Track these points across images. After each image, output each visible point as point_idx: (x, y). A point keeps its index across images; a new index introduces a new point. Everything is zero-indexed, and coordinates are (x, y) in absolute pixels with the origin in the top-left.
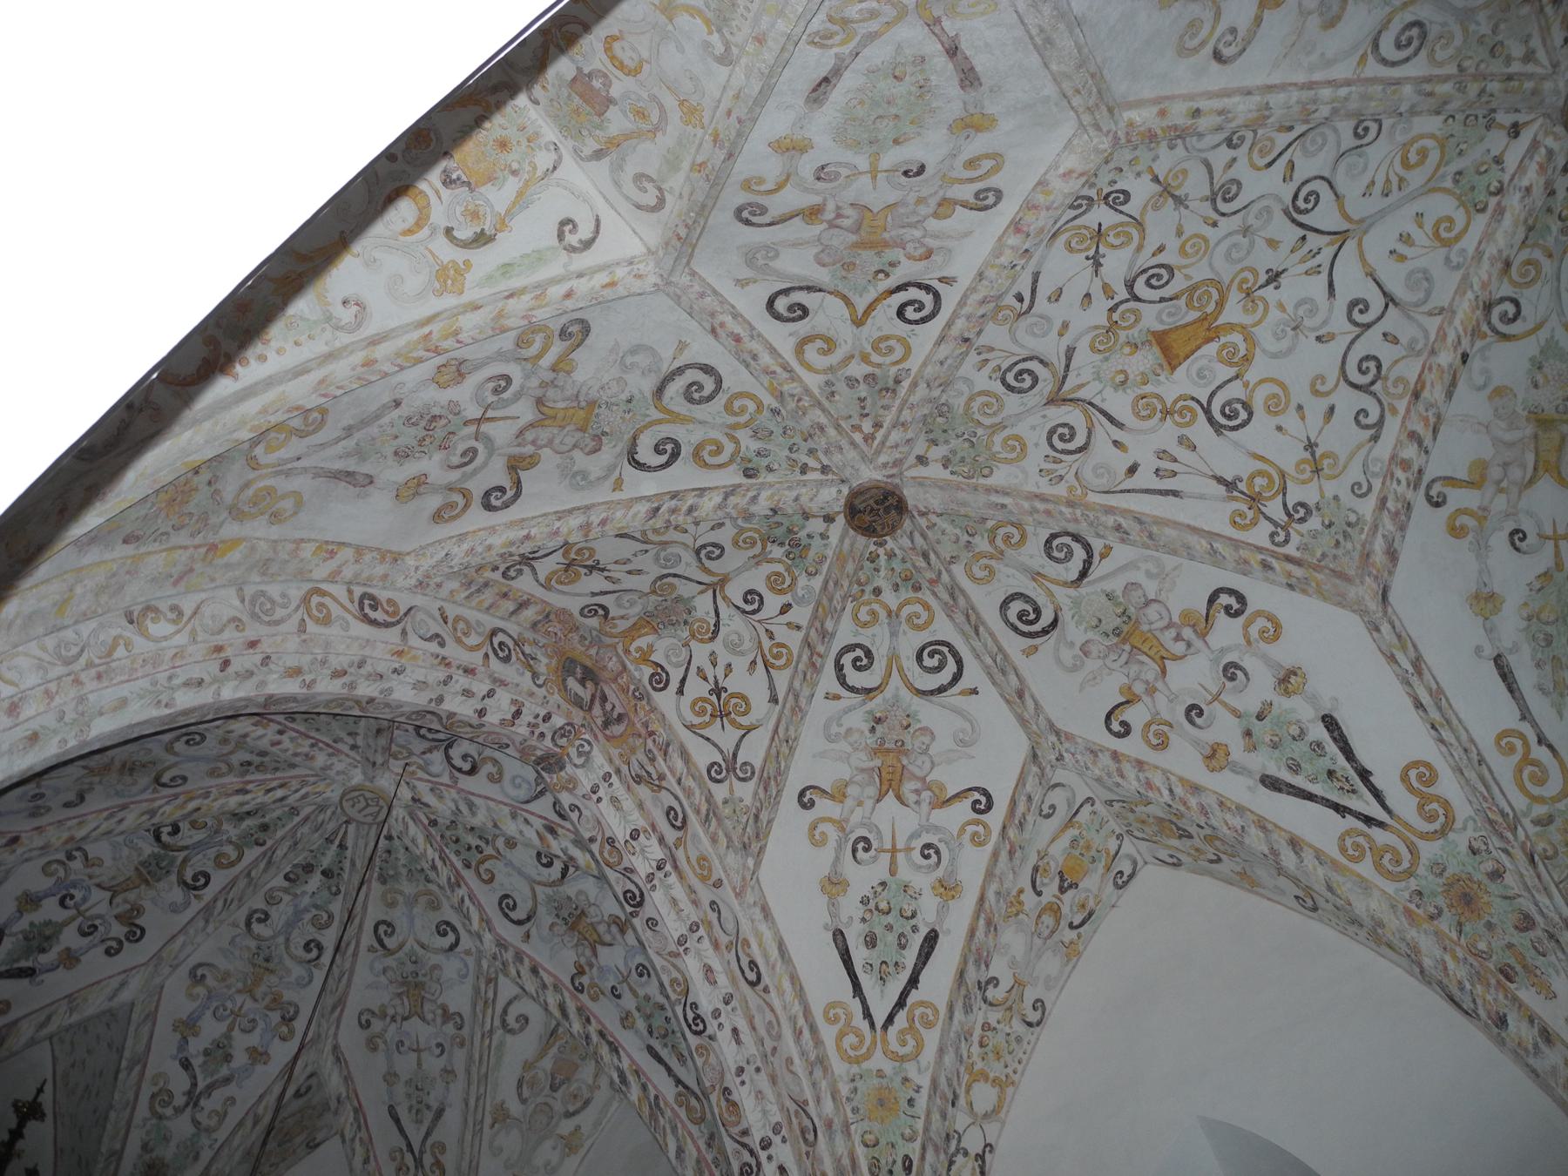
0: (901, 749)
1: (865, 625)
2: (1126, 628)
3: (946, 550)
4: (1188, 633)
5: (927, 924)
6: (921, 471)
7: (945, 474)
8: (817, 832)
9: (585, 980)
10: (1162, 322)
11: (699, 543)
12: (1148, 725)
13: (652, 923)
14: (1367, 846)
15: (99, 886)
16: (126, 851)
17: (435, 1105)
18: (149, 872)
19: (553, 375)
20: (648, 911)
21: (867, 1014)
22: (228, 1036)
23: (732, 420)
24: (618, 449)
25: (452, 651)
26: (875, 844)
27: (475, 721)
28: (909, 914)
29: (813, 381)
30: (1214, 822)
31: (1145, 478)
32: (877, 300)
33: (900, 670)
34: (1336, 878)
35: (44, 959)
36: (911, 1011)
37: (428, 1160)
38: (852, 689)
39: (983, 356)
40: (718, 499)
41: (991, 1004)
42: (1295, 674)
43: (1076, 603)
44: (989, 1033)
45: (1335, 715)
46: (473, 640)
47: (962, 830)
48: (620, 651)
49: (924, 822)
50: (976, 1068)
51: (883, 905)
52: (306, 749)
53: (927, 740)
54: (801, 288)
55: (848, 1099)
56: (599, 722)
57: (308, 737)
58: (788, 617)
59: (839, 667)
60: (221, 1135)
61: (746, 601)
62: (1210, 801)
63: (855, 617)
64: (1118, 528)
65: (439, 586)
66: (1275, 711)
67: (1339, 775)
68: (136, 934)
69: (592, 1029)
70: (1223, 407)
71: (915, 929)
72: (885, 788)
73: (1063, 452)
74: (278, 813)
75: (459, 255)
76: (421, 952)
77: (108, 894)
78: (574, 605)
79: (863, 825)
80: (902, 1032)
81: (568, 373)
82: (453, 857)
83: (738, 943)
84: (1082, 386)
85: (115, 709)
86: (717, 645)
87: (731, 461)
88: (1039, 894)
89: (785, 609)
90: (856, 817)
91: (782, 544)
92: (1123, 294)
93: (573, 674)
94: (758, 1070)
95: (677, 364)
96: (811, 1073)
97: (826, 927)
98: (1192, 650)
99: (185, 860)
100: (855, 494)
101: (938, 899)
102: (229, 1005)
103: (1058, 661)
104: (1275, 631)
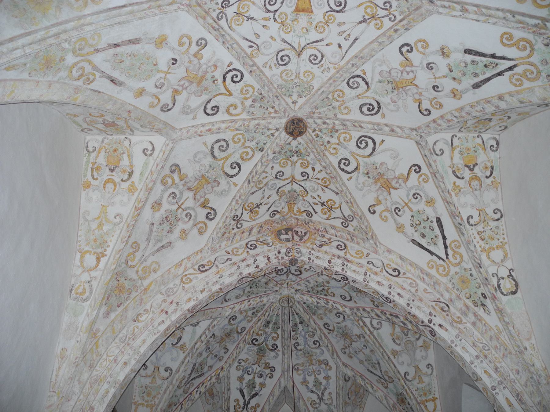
0: (381, 175)
1: (336, 153)
2: (394, 85)
3: (331, 115)
4: (408, 69)
5: (433, 217)
6: (298, 106)
7: (304, 99)
8: (383, 217)
9: (376, 303)
10: (291, 7)
11: (274, 176)
12: (431, 104)
13: (354, 281)
14: (519, 77)
15: (253, 364)
16: (251, 353)
17: (376, 362)
18: (261, 353)
19: (183, 181)
20: (350, 280)
21: (440, 258)
22: (316, 378)
23: (240, 144)
24: (224, 178)
25: (235, 259)
26: (400, 207)
27: (259, 270)
28: (426, 219)
29: (244, 116)
30: (474, 115)
31: (345, 45)
32: (225, 87)
33: (358, 155)
34: (520, 96)
35: (257, 389)
36: (451, 247)
37: (386, 378)
38: (352, 172)
39: (268, 66)
40: (260, 164)
41: (475, 225)
42: (443, 49)
43: (376, 92)
44: (482, 234)
45: (467, 48)
46: (241, 251)
47: (419, 182)
48: (294, 216)
49: (407, 189)
50: (486, 248)
51: (418, 223)
52: (259, 300)
53: (385, 166)
54: (206, 104)
55: (453, 288)
56: (298, 240)
57: (257, 297)
58: (317, 170)
59: (343, 170)
60: (335, 403)
61: (304, 177)
62: (468, 108)
63: (332, 154)
64: (353, 65)
65: (220, 246)
66: (452, 65)
67: (488, 64)
68: (273, 369)
69: (388, 315)
70: (335, 4)
71: (432, 222)
72: (388, 189)
73: (320, 62)
74: (274, 318)
75: (129, 183)
76: (339, 325)
77: (257, 365)
78: (267, 217)
79: (392, 205)
80: (453, 255)
81: (187, 177)
82: (321, 296)
83: (384, 268)
84: (299, 43)
85: (143, 343)
86: (310, 194)
87: (254, 152)
88: (463, 178)
89: (313, 169)
90: (389, 204)
91: (293, 156)
92: (271, 15)
93: (282, 234)
94: (413, 301)
95: (209, 148)
96: (435, 289)
97: (408, 242)
98: (415, 72)
99: (266, 345)
100: (286, 129)
101: (430, 207)
102: (309, 370)
103: (392, 111)
104: (426, 44)
